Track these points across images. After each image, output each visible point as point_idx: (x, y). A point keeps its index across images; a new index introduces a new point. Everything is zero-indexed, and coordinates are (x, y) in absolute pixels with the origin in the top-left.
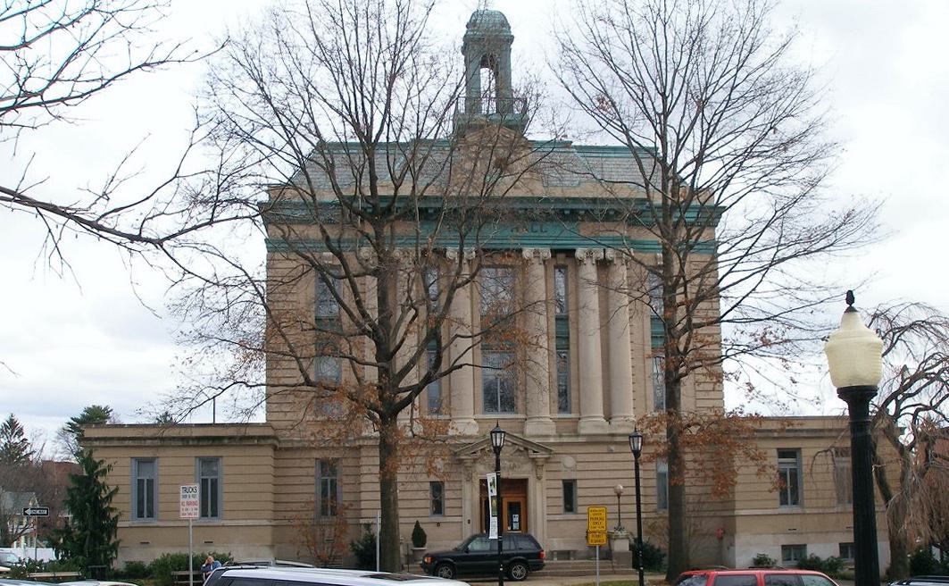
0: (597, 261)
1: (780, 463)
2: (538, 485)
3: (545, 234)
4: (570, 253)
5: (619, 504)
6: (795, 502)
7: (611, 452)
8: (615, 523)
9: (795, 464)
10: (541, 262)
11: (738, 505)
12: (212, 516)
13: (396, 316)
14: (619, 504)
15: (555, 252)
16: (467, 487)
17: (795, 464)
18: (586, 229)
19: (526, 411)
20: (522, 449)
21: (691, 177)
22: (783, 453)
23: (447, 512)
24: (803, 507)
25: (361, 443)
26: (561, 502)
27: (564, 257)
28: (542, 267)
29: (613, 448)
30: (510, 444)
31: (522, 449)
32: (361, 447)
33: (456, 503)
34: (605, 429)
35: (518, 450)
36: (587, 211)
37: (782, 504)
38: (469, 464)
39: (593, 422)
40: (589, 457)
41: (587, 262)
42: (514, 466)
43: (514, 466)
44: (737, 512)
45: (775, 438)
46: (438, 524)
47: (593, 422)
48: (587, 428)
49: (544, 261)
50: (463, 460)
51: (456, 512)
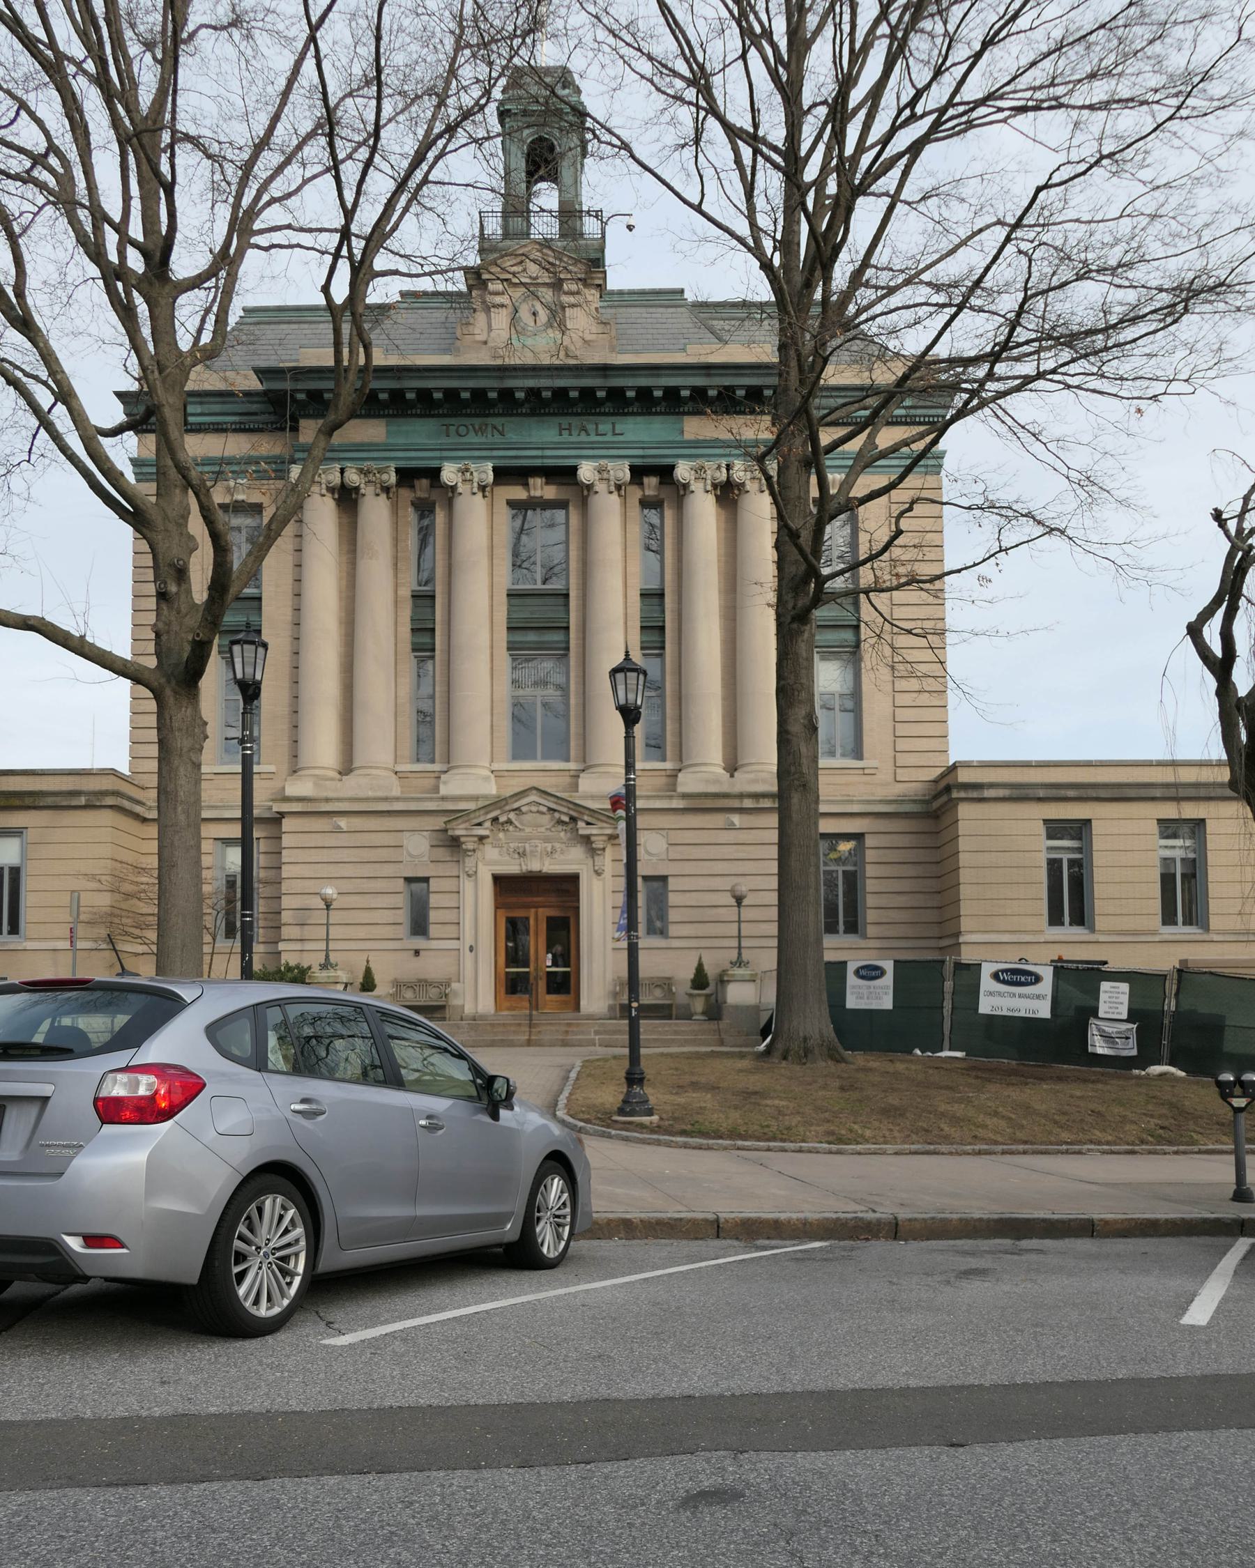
0: (715, 486)
1: (1050, 849)
2: (597, 884)
3: (621, 438)
4: (665, 473)
5: (739, 922)
6: (1188, 921)
7: (731, 827)
8: (734, 955)
9: (1079, 850)
10: (613, 488)
11: (965, 924)
12: (10, 933)
13: (330, 1336)
14: (739, 922)
15: (638, 473)
16: (467, 886)
17: (1079, 850)
18: (696, 428)
19: (584, 758)
20: (566, 819)
21: (826, 412)
22: (1055, 829)
23: (433, 930)
24: (1092, 929)
25: (285, 807)
26: (1044, 907)
27: (656, 481)
28: (615, 497)
29: (736, 819)
30: (545, 809)
31: (566, 819)
32: (282, 815)
33: (449, 916)
34: (725, 783)
35: (560, 822)
36: (694, 389)
37: (1164, 923)
38: (470, 846)
39: (707, 768)
40: (689, 837)
41: (697, 487)
42: (553, 851)
43: (553, 851)
44: (961, 940)
45: (1040, 799)
46: (417, 953)
47: (707, 768)
48: (689, 783)
49: (618, 487)
50: (459, 837)
51: (451, 931)
